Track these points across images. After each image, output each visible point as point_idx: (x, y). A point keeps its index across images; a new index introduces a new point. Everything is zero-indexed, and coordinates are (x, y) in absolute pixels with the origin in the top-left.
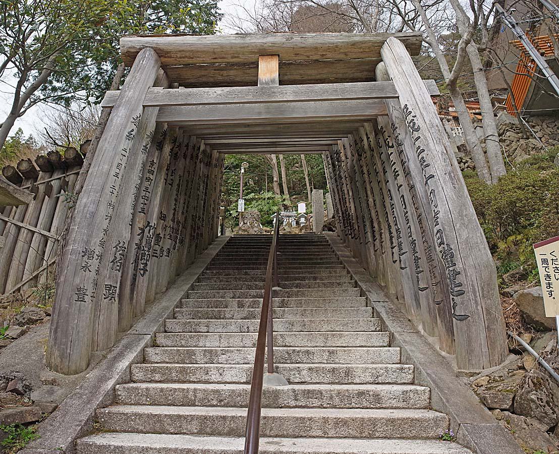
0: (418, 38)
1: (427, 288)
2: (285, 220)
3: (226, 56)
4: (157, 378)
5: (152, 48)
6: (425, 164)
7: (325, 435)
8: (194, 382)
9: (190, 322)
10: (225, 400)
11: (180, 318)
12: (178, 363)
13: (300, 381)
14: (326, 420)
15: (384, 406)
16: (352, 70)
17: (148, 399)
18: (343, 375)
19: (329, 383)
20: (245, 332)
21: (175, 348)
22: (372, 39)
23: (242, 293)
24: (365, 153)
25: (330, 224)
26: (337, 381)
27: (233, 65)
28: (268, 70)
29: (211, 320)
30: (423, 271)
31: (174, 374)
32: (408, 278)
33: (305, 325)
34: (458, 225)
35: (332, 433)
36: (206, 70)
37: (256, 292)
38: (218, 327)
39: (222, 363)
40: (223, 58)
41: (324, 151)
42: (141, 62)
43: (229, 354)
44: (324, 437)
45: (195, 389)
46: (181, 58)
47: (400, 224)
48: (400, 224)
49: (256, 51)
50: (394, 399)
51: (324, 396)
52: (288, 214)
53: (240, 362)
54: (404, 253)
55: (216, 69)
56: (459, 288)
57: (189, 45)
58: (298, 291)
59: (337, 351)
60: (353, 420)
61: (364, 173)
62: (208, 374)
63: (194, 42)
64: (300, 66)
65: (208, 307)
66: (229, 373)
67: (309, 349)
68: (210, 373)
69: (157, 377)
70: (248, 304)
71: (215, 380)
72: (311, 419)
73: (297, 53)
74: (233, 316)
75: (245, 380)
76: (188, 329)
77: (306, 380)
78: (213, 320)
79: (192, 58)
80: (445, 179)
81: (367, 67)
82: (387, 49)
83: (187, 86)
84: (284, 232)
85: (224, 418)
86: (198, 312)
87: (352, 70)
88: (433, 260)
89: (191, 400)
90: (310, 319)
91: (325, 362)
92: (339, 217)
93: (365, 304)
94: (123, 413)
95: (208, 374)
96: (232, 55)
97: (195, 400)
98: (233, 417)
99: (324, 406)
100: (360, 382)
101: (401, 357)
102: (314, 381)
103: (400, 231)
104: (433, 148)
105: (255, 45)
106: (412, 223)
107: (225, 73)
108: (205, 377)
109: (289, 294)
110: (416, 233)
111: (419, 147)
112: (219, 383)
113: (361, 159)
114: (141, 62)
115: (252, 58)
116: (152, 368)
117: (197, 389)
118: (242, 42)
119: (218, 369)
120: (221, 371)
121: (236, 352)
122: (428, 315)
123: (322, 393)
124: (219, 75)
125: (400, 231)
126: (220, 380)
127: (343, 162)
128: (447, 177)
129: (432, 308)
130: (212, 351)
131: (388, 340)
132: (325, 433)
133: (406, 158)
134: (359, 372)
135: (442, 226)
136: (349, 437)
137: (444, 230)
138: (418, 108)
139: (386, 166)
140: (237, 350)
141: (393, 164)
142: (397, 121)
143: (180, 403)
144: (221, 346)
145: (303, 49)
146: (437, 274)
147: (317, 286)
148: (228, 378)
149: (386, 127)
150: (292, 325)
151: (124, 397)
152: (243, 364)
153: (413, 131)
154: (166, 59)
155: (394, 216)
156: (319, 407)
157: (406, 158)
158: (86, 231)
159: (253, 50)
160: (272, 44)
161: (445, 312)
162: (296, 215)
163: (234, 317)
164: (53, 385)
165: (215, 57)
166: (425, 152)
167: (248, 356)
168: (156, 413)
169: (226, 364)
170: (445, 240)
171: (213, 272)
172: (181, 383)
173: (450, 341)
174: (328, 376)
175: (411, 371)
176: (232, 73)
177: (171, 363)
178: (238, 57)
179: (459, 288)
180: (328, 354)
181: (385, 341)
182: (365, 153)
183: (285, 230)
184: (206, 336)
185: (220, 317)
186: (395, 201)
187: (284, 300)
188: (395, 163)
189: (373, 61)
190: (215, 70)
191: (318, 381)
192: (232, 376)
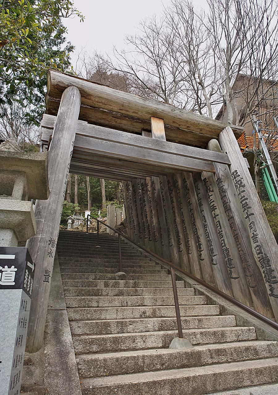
0: (241, 131)
1: (238, 278)
2: (76, 222)
3: (130, 110)
4: (94, 349)
5: (78, 87)
6: (248, 206)
7: (252, 384)
8: (124, 350)
9: (84, 299)
10: (166, 363)
11: (67, 295)
12: (96, 334)
13: (197, 343)
14: (250, 371)
15: (260, 357)
16: (195, 140)
17: (106, 370)
18: (220, 336)
19: (214, 343)
20: (125, 306)
21: (94, 321)
22: (218, 125)
23: (101, 276)
24: (179, 190)
25: (119, 229)
26: (217, 341)
27: (125, 117)
28: (158, 128)
29: (101, 297)
30: (235, 267)
31: (108, 344)
32: (219, 270)
33: (164, 301)
34: (270, 244)
35: (256, 382)
36: (107, 115)
37: (111, 275)
38: (106, 302)
39: (130, 332)
40: (127, 111)
41: (123, 180)
42: (72, 97)
43: (135, 324)
44: (252, 386)
45: (144, 356)
46: (97, 102)
47: (211, 237)
48: (211, 237)
49: (151, 112)
50: (264, 351)
51: (228, 353)
52: (77, 217)
53: (143, 331)
54: (215, 255)
55: (114, 116)
56: (274, 279)
57: (106, 94)
58: (139, 275)
59: (202, 319)
60: (265, 369)
61: (174, 202)
62: (134, 342)
63: (110, 93)
64: (168, 129)
65: (82, 287)
66: (150, 340)
67: (186, 318)
68: (136, 341)
69: (95, 348)
70: (111, 284)
71: (140, 347)
72: (242, 372)
73: (175, 121)
74: (108, 294)
75: (161, 345)
76: (83, 304)
77: (200, 342)
78: (102, 297)
79: (106, 105)
80: (260, 217)
81: (204, 140)
82: (226, 133)
83: (90, 122)
84: (78, 230)
85: (188, 379)
86: (82, 290)
87: (195, 140)
88: (248, 262)
89: (141, 366)
90: (167, 297)
91: (197, 327)
92: (134, 225)
93: (184, 286)
94: (106, 387)
95: (134, 342)
96: (134, 111)
97: (143, 366)
98: (194, 377)
99: (229, 361)
100: (230, 341)
101: (236, 321)
102: (205, 343)
103: (212, 241)
104: (253, 199)
105: (152, 108)
106: (225, 237)
107: (119, 121)
108: (133, 345)
109: (133, 277)
110: (229, 244)
111: (244, 196)
112: (143, 349)
113: (172, 193)
114: (72, 97)
115: (148, 116)
116: (90, 340)
117: (145, 356)
118: (143, 103)
119: (142, 337)
120: (144, 339)
121: (140, 322)
122: (241, 294)
123: (226, 351)
124: (115, 121)
125: (212, 241)
126: (144, 346)
127: (150, 191)
128: (261, 215)
129: (243, 290)
130: (122, 322)
131: (219, 310)
132: (252, 382)
133: (228, 200)
134: (228, 334)
135: (261, 243)
136: (266, 384)
137: (262, 245)
138: (244, 174)
139: (202, 201)
140: (141, 321)
141: (212, 202)
142: (222, 177)
143: (132, 370)
144: (118, 318)
145: (179, 120)
146: (251, 270)
147: (145, 272)
148: (149, 345)
149: (209, 179)
150: (156, 301)
151: (84, 371)
152: (145, 332)
153: (240, 186)
154: (86, 100)
155: (206, 232)
156: (226, 362)
157: (228, 200)
158: (51, 224)
159: (149, 112)
160: (162, 110)
161: (259, 293)
162: (84, 219)
163: (109, 294)
164: (28, 365)
165: (122, 108)
166: (248, 200)
167: (149, 325)
168: (135, 382)
169: (133, 333)
170: (263, 251)
171: (65, 259)
172: (113, 352)
173: (266, 311)
174: (212, 338)
175: (254, 331)
176: (124, 122)
177: (90, 334)
178: (137, 113)
179: (274, 279)
180: (198, 322)
181: (218, 311)
182: (179, 190)
183: (78, 229)
184: (107, 310)
185: (98, 294)
186: (208, 223)
187: (136, 282)
188: (214, 201)
189: (208, 137)
190: (113, 117)
191: (207, 342)
192: (152, 342)
